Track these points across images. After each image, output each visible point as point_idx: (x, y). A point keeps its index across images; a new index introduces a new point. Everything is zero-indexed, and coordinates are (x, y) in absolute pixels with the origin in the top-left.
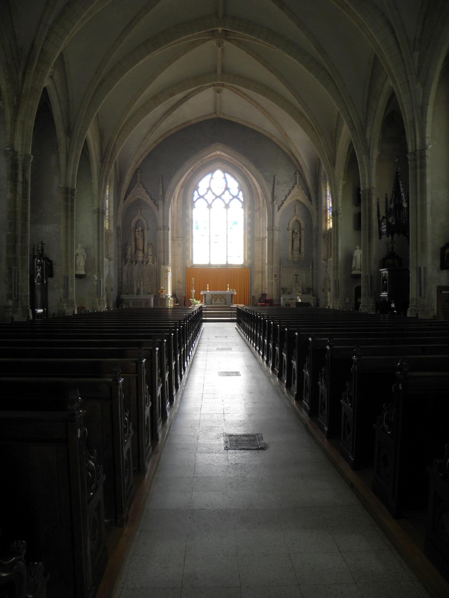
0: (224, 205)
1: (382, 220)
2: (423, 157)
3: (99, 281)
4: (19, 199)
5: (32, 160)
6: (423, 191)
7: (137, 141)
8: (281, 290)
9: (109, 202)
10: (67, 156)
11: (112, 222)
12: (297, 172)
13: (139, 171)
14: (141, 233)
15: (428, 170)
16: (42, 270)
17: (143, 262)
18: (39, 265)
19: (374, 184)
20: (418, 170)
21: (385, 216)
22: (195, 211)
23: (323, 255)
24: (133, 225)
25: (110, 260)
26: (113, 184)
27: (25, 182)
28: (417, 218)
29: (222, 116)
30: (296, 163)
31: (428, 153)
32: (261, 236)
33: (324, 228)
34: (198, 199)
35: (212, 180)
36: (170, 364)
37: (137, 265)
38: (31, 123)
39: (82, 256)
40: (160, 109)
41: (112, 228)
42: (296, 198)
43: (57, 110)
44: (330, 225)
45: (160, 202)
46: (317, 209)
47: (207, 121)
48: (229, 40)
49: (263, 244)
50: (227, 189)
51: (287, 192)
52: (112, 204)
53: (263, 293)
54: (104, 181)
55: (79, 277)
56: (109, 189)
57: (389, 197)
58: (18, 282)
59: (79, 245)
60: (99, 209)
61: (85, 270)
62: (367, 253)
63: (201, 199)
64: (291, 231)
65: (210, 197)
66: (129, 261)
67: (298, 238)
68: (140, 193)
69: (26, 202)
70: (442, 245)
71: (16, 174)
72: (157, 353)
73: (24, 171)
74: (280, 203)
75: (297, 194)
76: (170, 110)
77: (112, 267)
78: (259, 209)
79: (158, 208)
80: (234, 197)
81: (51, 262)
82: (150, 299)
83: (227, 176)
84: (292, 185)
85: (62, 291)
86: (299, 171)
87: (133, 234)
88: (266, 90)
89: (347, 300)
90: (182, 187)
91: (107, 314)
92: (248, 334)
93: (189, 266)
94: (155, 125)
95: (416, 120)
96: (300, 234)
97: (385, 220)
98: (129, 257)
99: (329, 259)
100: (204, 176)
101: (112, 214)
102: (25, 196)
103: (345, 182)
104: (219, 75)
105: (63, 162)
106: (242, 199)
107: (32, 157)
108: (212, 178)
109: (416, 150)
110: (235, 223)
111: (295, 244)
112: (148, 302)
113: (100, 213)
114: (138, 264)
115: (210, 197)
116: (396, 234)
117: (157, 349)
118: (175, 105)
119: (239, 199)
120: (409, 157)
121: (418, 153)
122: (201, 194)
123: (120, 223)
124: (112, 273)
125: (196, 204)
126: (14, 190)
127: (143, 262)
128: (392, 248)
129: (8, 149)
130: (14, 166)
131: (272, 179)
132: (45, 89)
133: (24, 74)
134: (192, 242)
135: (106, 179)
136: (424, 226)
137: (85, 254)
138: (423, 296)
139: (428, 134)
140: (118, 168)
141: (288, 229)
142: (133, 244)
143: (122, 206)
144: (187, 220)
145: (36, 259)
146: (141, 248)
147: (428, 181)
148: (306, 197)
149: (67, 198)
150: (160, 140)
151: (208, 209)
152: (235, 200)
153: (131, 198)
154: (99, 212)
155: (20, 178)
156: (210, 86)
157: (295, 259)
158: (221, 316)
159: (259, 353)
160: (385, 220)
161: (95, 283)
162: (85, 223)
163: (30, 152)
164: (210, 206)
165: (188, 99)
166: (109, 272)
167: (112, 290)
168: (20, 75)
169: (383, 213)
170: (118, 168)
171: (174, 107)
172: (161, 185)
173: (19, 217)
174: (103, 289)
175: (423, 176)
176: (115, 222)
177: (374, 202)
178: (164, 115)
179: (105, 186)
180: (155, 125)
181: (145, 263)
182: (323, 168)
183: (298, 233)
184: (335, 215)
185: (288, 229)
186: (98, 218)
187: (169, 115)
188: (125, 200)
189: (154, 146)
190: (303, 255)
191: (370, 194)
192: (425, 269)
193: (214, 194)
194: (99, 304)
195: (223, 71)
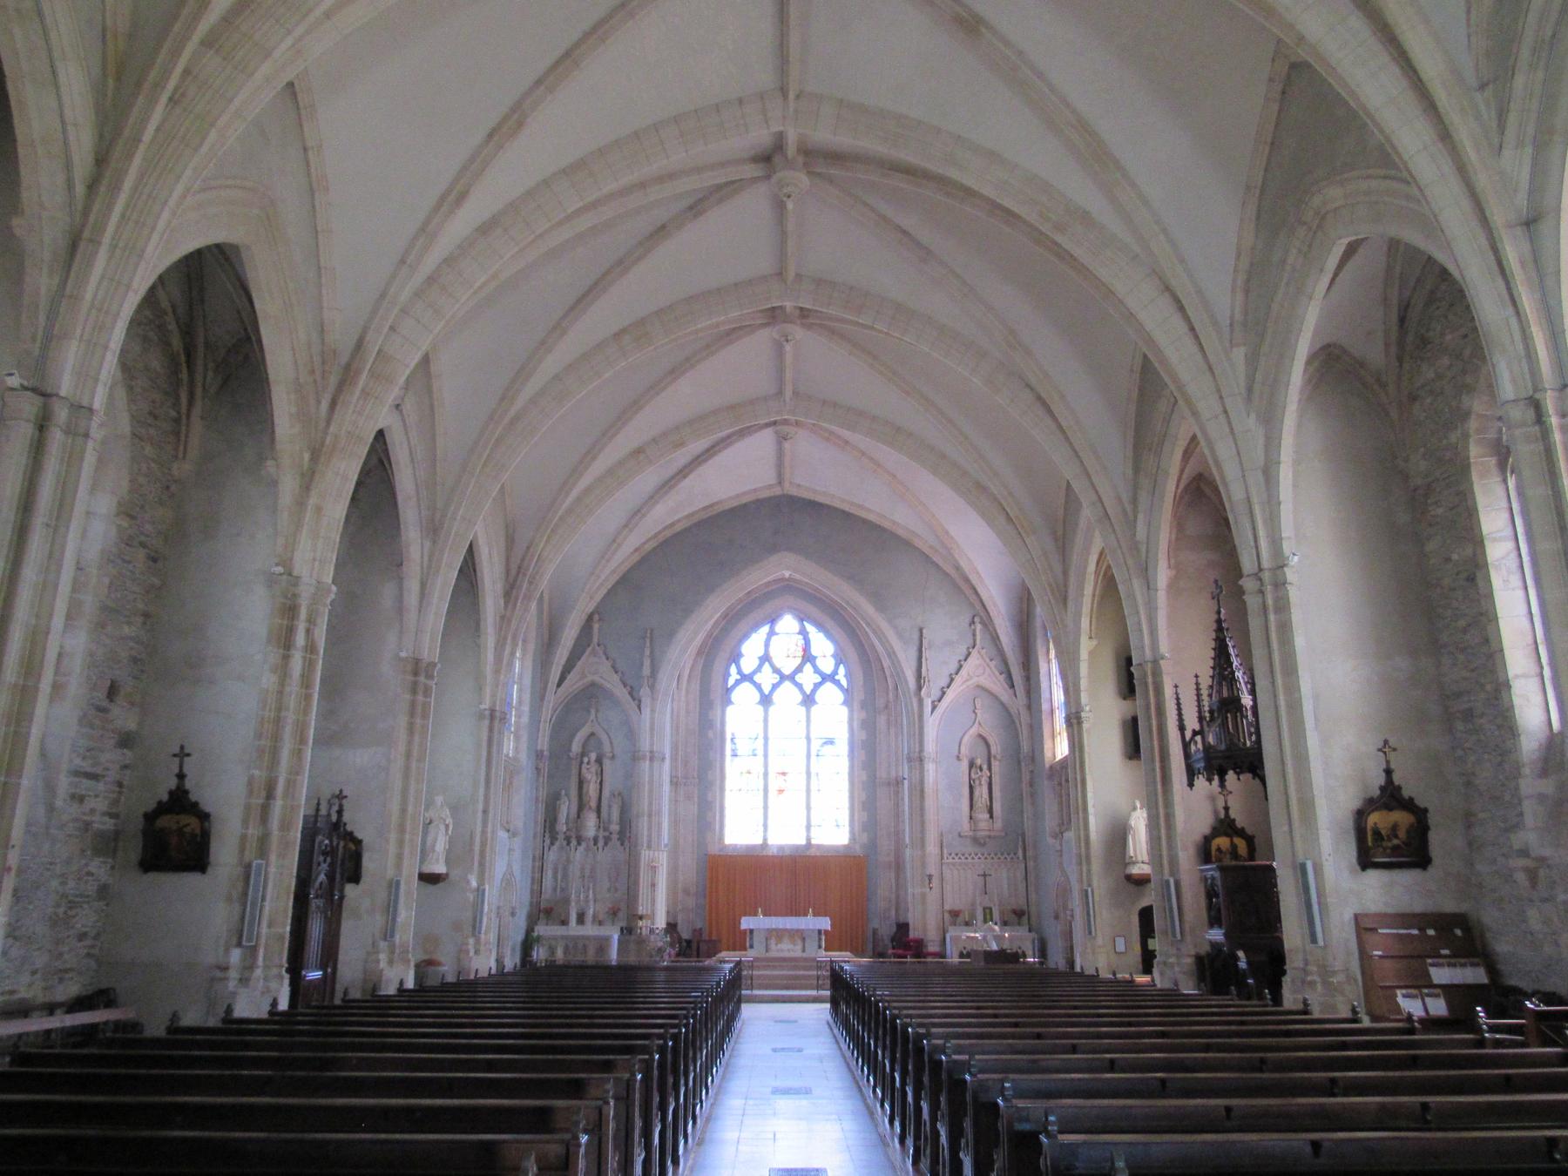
0: (800, 697)
1: (1192, 738)
2: (1280, 585)
3: (480, 892)
4: (294, 687)
5: (333, 596)
6: (1291, 669)
7: (591, 550)
8: (947, 916)
9: (520, 690)
10: (423, 585)
11: (525, 738)
12: (977, 619)
13: (596, 617)
14: (594, 768)
15: (1296, 616)
16: (332, 865)
17: (596, 840)
18: (325, 853)
19: (1164, 648)
20: (1272, 617)
21: (1197, 728)
22: (730, 711)
23: (1050, 821)
24: (576, 747)
25: (513, 834)
26: (531, 647)
27: (311, 648)
28: (1280, 735)
29: (794, 492)
30: (973, 598)
31: (1290, 575)
32: (893, 774)
33: (1048, 754)
34: (737, 683)
35: (774, 638)
36: (663, 1108)
37: (581, 848)
38: (337, 510)
39: (442, 827)
40: (649, 479)
41: (523, 757)
42: (974, 681)
43: (405, 480)
44: (1060, 748)
45: (644, 692)
46: (1029, 707)
47: (759, 503)
48: (809, 327)
49: (897, 793)
50: (808, 657)
51: (953, 667)
52: (527, 697)
53: (902, 920)
54: (509, 641)
55: (430, 879)
56: (522, 659)
57: (1205, 682)
58: (263, 899)
59: (439, 799)
60: (492, 711)
61: (447, 862)
62: (1161, 823)
63: (746, 685)
64: (965, 764)
65: (766, 678)
66: (561, 837)
67: (984, 781)
68: (594, 668)
69: (308, 697)
70: (1356, 804)
71: (291, 630)
72: (582, 1150)
73: (311, 621)
74: (936, 693)
75: (980, 671)
76: (673, 477)
77: (517, 854)
78: (886, 707)
79: (639, 707)
80: (825, 678)
81: (359, 842)
82: (607, 939)
83: (810, 628)
84: (963, 650)
85: (380, 919)
86: (981, 615)
87: (574, 771)
88: (896, 434)
89: (1121, 947)
90: (699, 653)
91: (498, 982)
92: (856, 1046)
93: (713, 849)
94: (638, 513)
95: (1255, 500)
96: (990, 769)
97: (1198, 738)
98: (562, 827)
99: (1066, 835)
100: (746, 636)
101: (525, 719)
102: (306, 682)
103: (1094, 642)
104: (781, 408)
105: (412, 599)
106: (844, 682)
107: (334, 588)
108: (772, 633)
109: (1261, 570)
110: (830, 742)
111: (977, 793)
112: (602, 945)
113: (495, 718)
114: (584, 845)
115: (766, 678)
116: (1231, 773)
117: (584, 1139)
118: (685, 467)
119: (837, 683)
120: (1248, 584)
121: (1266, 576)
122: (747, 670)
123: (544, 743)
124: (516, 868)
125: (734, 696)
126: (283, 670)
127: (596, 840)
128: (1227, 809)
129: (280, 569)
130: (290, 610)
131: (916, 636)
132: (380, 434)
133: (333, 404)
134: (722, 789)
135: (514, 638)
136: (1302, 758)
137: (449, 821)
138: (1321, 943)
139: (1287, 530)
140: (546, 607)
141: (958, 758)
142: (574, 792)
143: (551, 700)
144: (711, 734)
145: (320, 838)
146: (593, 804)
147: (1300, 642)
148: (1002, 678)
149: (415, 683)
150: (649, 547)
151: (761, 708)
152: (829, 685)
153: (574, 682)
154: (492, 717)
155: (300, 639)
156: (767, 425)
157: (980, 834)
158: (788, 983)
159: (882, 1106)
160: (1198, 738)
161: (471, 897)
162: (456, 743)
163: (328, 578)
164: (766, 700)
165: (715, 454)
166: (509, 865)
167: (513, 914)
168: (325, 405)
169: (1192, 723)
170: (546, 607)
171: (684, 472)
172: (647, 652)
173: (288, 732)
174: (490, 910)
175: (1285, 628)
176: (533, 737)
177: (1168, 692)
178: (663, 486)
179: (513, 654)
180: (638, 513)
181: (601, 843)
182: (1039, 610)
183: (985, 767)
184: (1074, 721)
185: (958, 758)
186: (491, 729)
187: (671, 488)
188: (559, 685)
189: (636, 558)
190: (998, 824)
191: (1157, 673)
192: (1318, 869)
193: (776, 671)
194: (477, 952)
195: (796, 394)
